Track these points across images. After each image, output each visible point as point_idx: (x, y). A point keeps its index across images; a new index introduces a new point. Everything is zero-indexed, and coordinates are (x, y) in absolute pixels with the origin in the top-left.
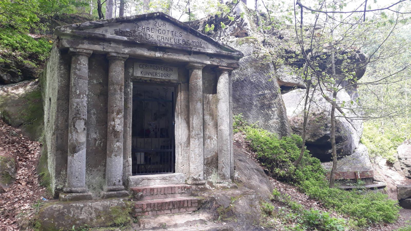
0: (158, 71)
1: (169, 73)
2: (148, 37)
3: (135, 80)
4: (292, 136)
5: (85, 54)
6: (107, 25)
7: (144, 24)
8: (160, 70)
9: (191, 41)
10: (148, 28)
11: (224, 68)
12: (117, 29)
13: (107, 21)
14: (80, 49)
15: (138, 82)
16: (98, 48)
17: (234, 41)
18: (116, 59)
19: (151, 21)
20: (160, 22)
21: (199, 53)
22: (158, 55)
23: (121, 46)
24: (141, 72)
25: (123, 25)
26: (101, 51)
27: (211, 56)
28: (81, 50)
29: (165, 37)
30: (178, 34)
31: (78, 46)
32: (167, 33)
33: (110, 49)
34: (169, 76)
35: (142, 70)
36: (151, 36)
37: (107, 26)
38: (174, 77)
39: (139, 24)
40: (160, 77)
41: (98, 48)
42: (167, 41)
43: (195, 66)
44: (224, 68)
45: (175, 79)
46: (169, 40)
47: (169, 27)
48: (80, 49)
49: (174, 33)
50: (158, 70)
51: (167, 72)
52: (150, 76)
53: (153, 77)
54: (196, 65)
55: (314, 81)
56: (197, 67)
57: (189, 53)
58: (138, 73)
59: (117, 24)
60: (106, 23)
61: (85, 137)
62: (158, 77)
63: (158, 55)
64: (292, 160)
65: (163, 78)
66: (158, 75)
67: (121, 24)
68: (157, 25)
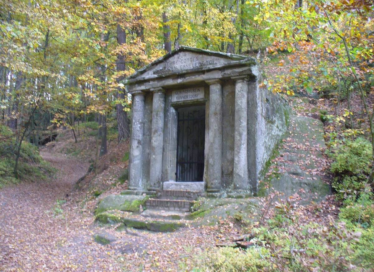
0: (189, 94)
1: (197, 93)
2: (174, 69)
4: (350, 146)
9: (205, 61)
12: (154, 70)
15: (177, 107)
16: (143, 87)
19: (176, 56)
20: (181, 54)
21: (209, 71)
22: (180, 81)
23: (156, 82)
27: (222, 69)
30: (195, 59)
31: (132, 89)
32: (187, 61)
35: (177, 96)
38: (200, 96)
39: (168, 61)
40: (190, 99)
41: (143, 87)
47: (189, 55)
49: (192, 59)
52: (183, 100)
53: (185, 100)
54: (210, 81)
55: (72, 171)
57: (203, 72)
58: (175, 98)
61: (246, 121)
63: (180, 81)
65: (193, 99)
68: (180, 57)
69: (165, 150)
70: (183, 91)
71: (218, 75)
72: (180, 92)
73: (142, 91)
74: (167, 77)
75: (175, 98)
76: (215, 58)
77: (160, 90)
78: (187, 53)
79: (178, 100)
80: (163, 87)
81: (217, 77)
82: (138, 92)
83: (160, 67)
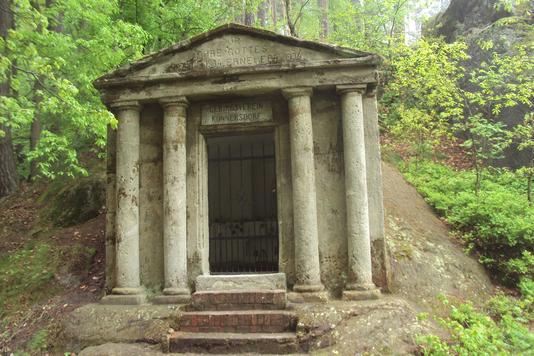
1: (171, 177)
3: (207, 132)
5: (129, 107)
6: (154, 61)
7: (205, 48)
8: (242, 109)
10: (213, 52)
11: (348, 87)
13: (151, 57)
14: (122, 101)
16: (143, 95)
17: (143, 49)
18: (169, 106)
20: (229, 39)
22: (227, 87)
24: (213, 118)
25: (177, 56)
26: (147, 99)
27: (320, 70)
28: (124, 104)
29: (239, 58)
33: (158, 93)
34: (256, 116)
36: (217, 63)
37: (155, 63)
39: (199, 49)
41: (143, 95)
42: (243, 63)
43: (292, 93)
44: (348, 87)
45: (268, 119)
46: (246, 61)
48: (122, 101)
50: (239, 110)
51: (254, 111)
52: (226, 122)
53: (230, 122)
54: (293, 90)
56: (297, 94)
58: (209, 120)
59: (167, 57)
60: (151, 60)
62: (240, 121)
64: (471, 342)
66: (239, 118)
67: (174, 55)
69: (192, 215)
70: (227, 107)
71: (314, 81)
72: (220, 108)
73: (140, 101)
74: (201, 78)
75: (209, 120)
76: (303, 50)
77: (132, 107)
78: (242, 38)
79: (217, 123)
80: (187, 97)
81: (308, 84)
82: (132, 103)
83: (179, 59)
